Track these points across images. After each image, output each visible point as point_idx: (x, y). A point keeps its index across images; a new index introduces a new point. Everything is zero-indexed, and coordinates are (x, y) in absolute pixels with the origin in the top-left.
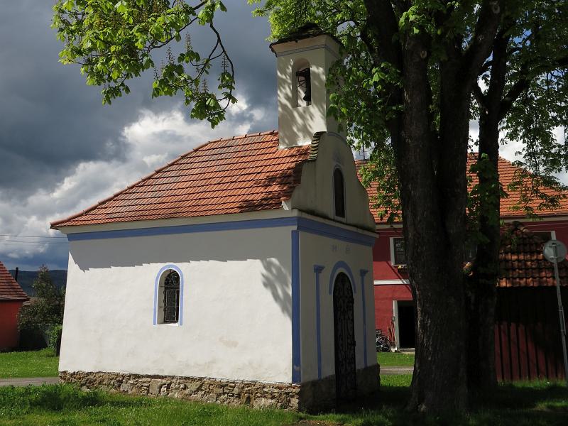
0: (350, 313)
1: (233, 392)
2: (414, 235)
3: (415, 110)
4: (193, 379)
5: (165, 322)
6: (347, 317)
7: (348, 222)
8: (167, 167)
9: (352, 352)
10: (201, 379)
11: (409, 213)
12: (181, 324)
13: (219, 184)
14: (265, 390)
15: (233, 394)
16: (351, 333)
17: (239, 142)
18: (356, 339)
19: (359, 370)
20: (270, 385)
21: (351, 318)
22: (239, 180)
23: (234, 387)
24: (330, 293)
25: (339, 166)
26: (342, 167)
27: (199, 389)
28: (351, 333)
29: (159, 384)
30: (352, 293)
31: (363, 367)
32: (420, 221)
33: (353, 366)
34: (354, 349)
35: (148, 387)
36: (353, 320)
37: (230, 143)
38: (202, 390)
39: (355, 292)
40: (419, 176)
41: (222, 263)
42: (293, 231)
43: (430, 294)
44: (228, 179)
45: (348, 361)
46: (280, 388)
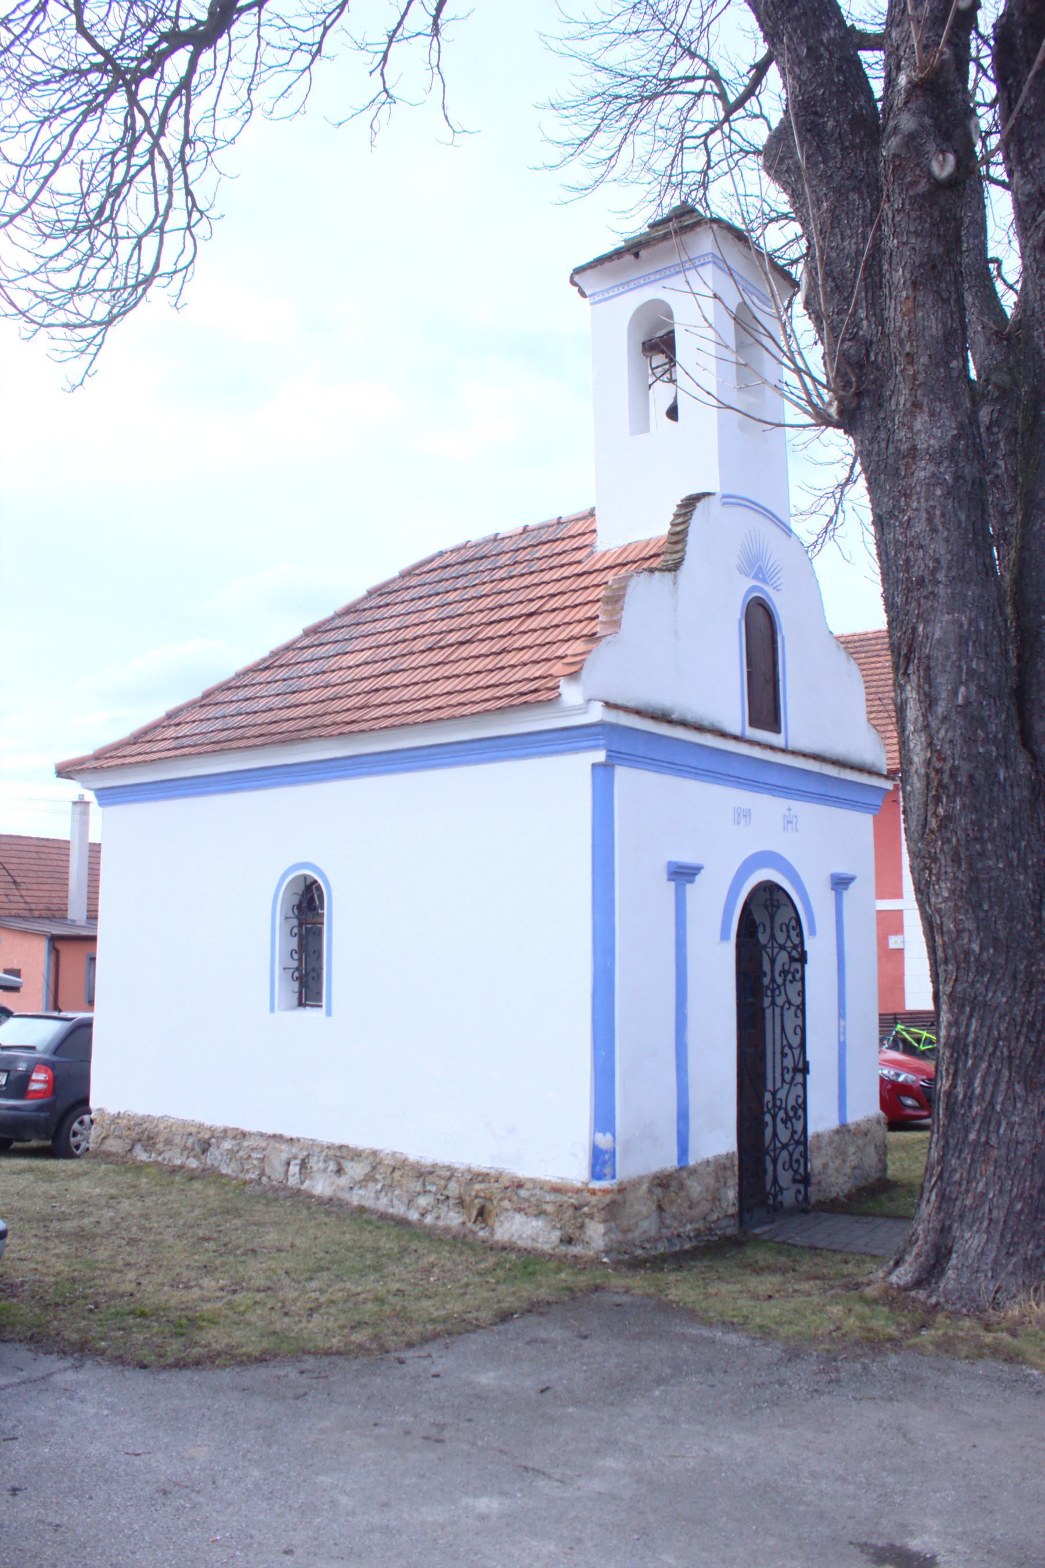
0: (792, 990)
1: (446, 1193)
2: (928, 763)
3: (925, 360)
4: (356, 1155)
5: (301, 1004)
6: (780, 1001)
7: (791, 746)
8: (332, 619)
9: (799, 1090)
10: (374, 1153)
11: (911, 693)
12: (329, 1013)
13: (431, 649)
14: (523, 1193)
15: (448, 1197)
16: (795, 1041)
17: (508, 545)
18: (809, 1058)
19: (818, 1136)
20: (533, 1181)
21: (797, 1001)
22: (480, 636)
23: (449, 1178)
24: (724, 936)
25: (761, 590)
26: (768, 589)
27: (369, 1178)
28: (795, 1041)
29: (285, 1156)
30: (800, 935)
31: (833, 1123)
32: (945, 719)
33: (799, 1126)
34: (804, 1086)
35: (262, 1160)
36: (802, 1008)
37: (485, 551)
38: (376, 1181)
39: (813, 932)
40: (941, 577)
41: (744, 858)
42: (594, 765)
43: (975, 947)
44: (452, 638)
45: (781, 1114)
46: (556, 1190)
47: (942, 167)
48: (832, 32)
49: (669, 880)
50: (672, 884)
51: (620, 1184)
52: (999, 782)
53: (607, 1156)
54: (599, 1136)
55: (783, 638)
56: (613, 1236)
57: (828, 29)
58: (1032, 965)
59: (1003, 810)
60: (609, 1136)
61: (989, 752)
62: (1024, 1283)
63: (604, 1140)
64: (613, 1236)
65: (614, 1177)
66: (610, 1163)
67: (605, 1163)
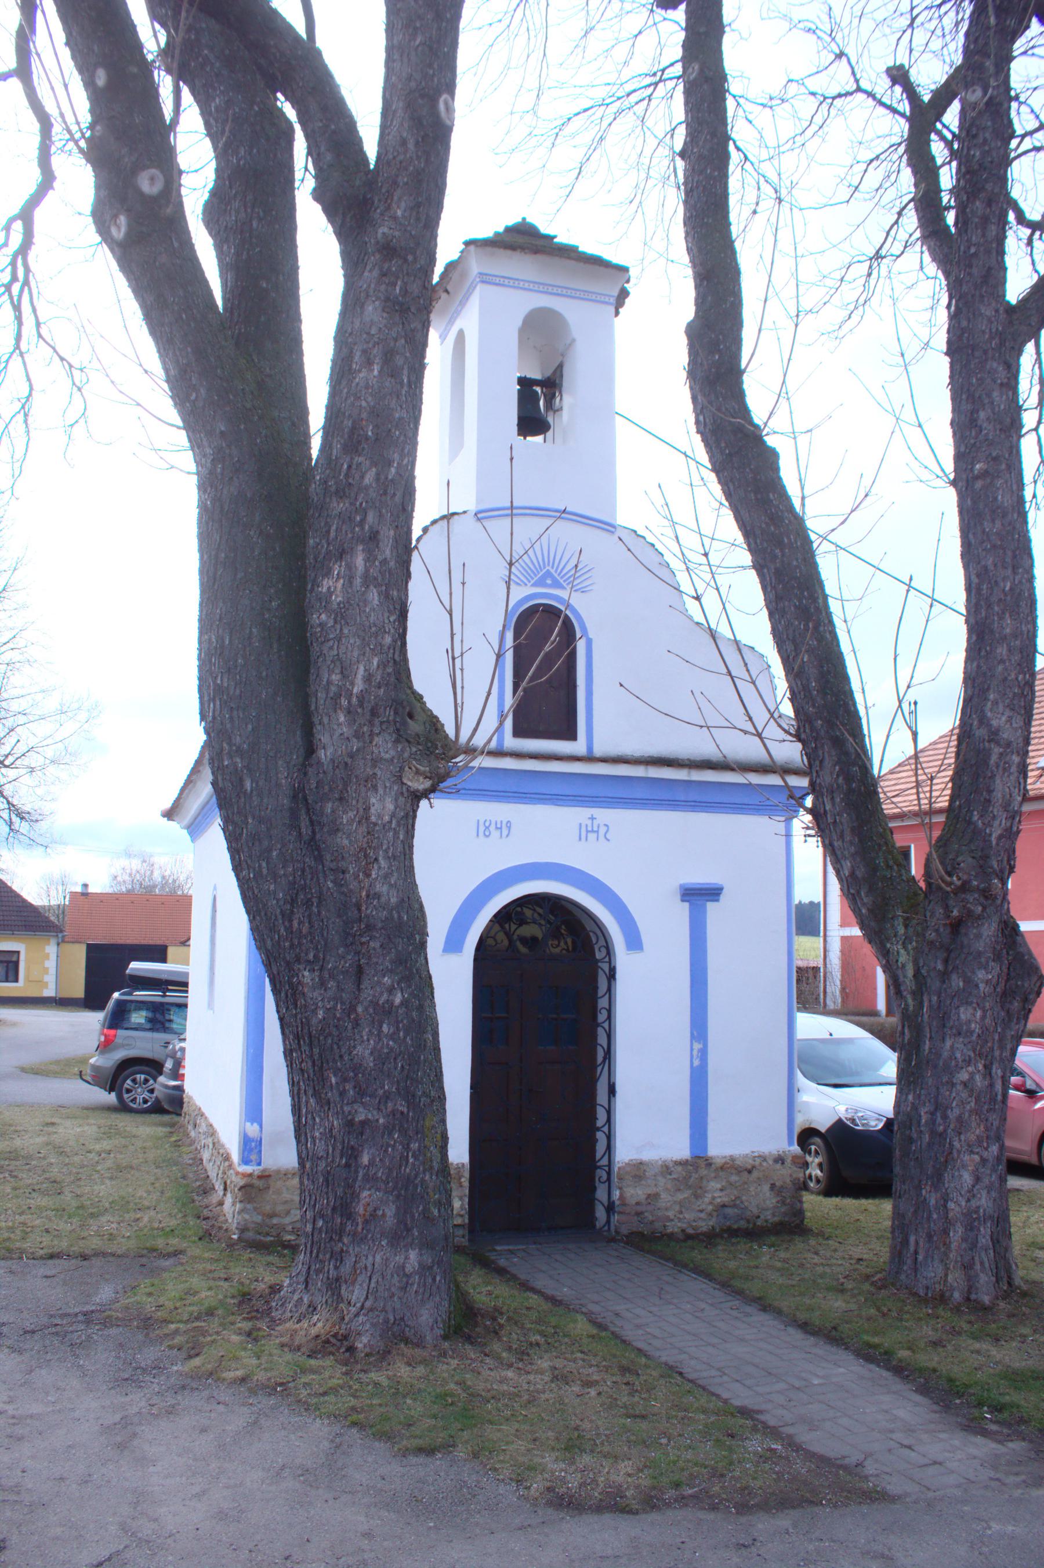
47: (119, 228)
48: (217, 101)
49: (683, 901)
50: (686, 905)
51: (264, 1170)
52: (245, 793)
53: (253, 1144)
54: (248, 1124)
55: (589, 643)
56: (247, 1217)
57: (214, 99)
58: (293, 977)
59: (250, 821)
60: (256, 1126)
61: (235, 764)
62: (326, 1301)
63: (252, 1129)
64: (247, 1217)
65: (259, 1164)
66: (256, 1151)
67: (251, 1150)
